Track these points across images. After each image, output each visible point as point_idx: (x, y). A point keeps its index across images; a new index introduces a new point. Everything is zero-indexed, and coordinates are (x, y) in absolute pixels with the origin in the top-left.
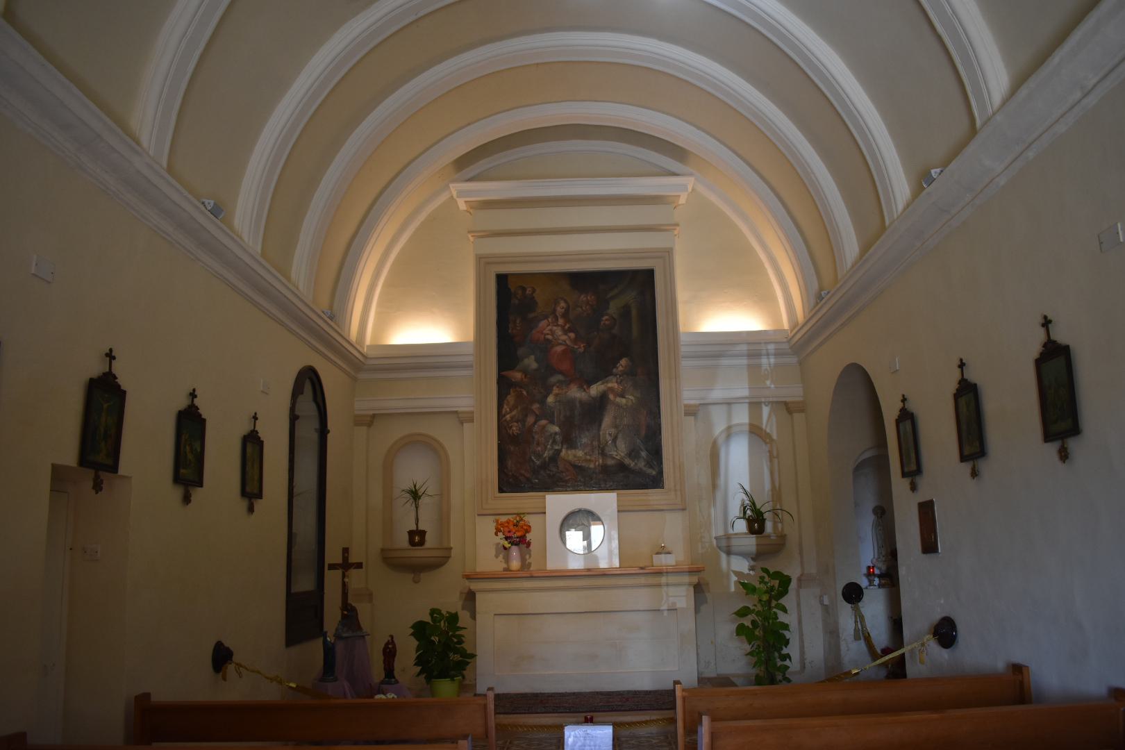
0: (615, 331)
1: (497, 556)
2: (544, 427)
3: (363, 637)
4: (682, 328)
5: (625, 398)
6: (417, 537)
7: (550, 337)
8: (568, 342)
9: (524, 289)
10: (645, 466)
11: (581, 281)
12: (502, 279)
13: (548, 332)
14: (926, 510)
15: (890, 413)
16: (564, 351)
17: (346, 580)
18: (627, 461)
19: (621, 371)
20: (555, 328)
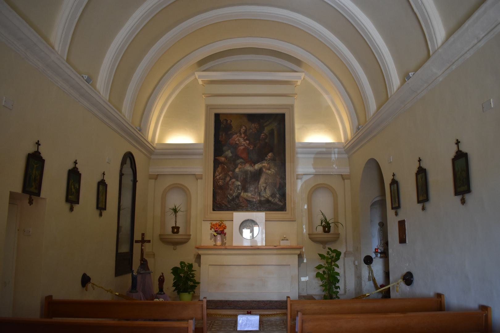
0: (267, 141)
1: (211, 239)
2: (233, 182)
3: (150, 273)
4: (297, 141)
5: (270, 170)
6: (176, 230)
7: (237, 142)
8: (246, 145)
9: (227, 120)
10: (278, 201)
11: (252, 117)
12: (217, 116)
13: (237, 140)
14: (402, 224)
15: (387, 181)
16: (244, 149)
17: (143, 248)
18: (270, 199)
19: (269, 158)
20: (240, 138)
